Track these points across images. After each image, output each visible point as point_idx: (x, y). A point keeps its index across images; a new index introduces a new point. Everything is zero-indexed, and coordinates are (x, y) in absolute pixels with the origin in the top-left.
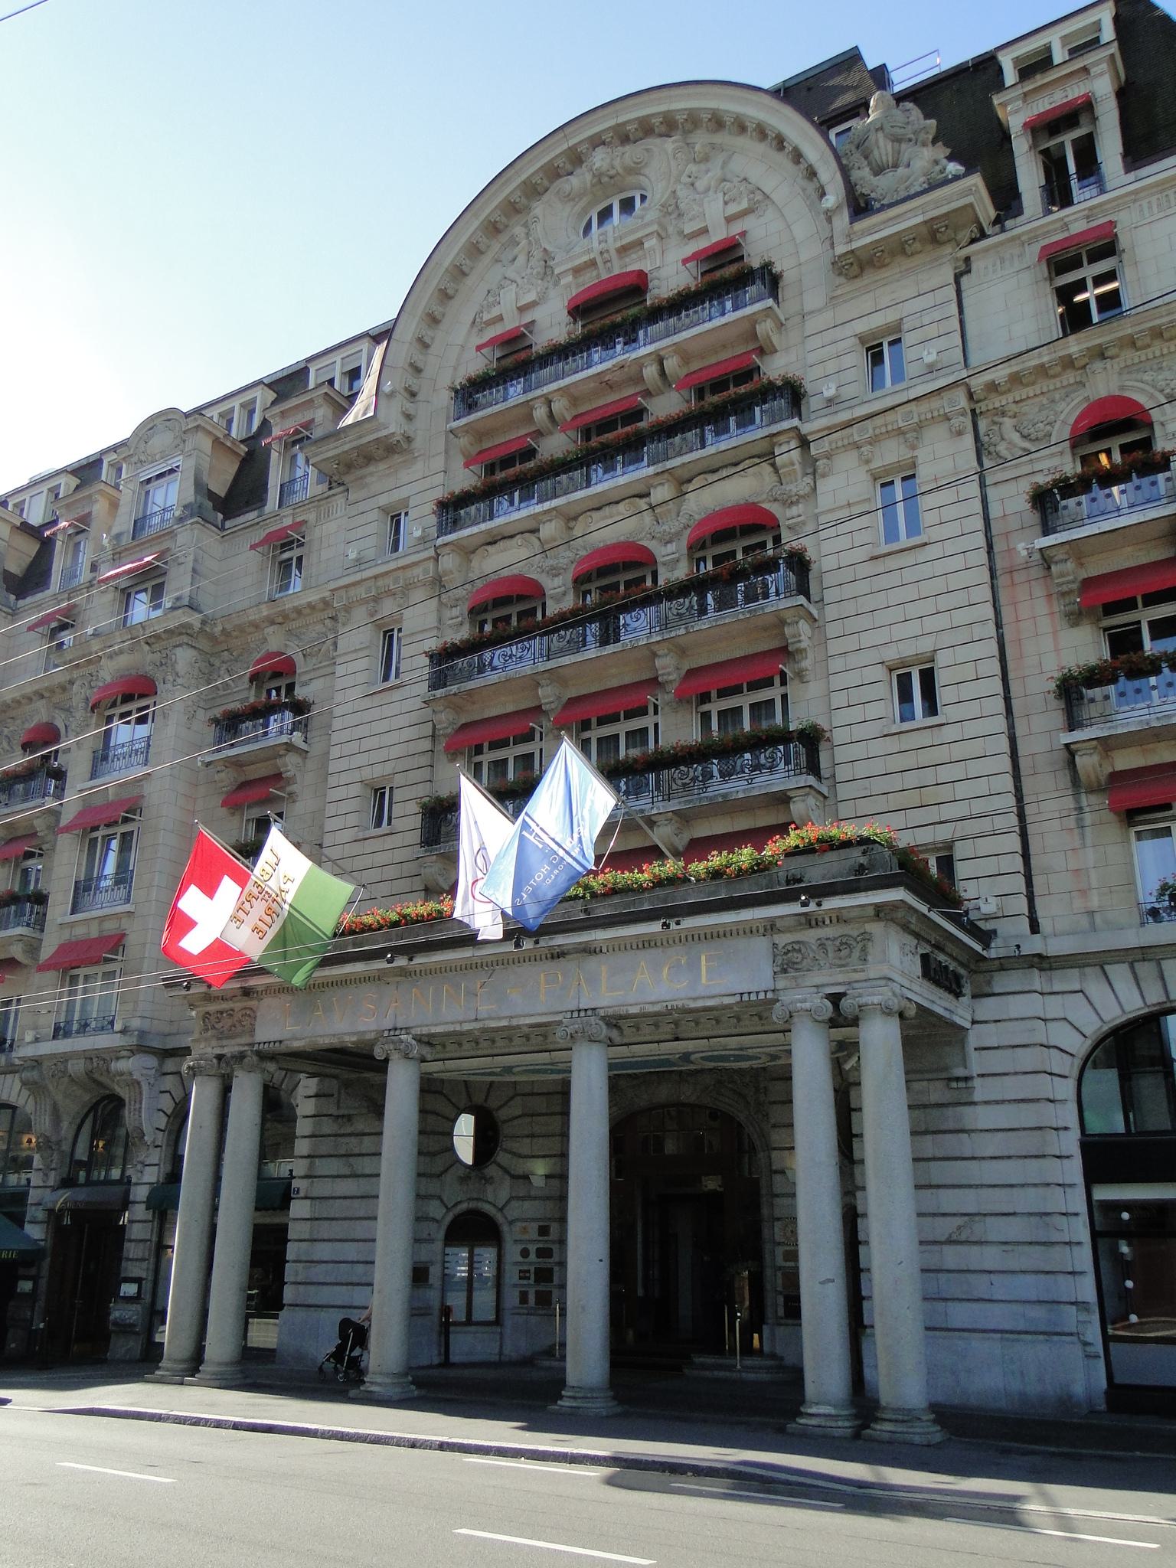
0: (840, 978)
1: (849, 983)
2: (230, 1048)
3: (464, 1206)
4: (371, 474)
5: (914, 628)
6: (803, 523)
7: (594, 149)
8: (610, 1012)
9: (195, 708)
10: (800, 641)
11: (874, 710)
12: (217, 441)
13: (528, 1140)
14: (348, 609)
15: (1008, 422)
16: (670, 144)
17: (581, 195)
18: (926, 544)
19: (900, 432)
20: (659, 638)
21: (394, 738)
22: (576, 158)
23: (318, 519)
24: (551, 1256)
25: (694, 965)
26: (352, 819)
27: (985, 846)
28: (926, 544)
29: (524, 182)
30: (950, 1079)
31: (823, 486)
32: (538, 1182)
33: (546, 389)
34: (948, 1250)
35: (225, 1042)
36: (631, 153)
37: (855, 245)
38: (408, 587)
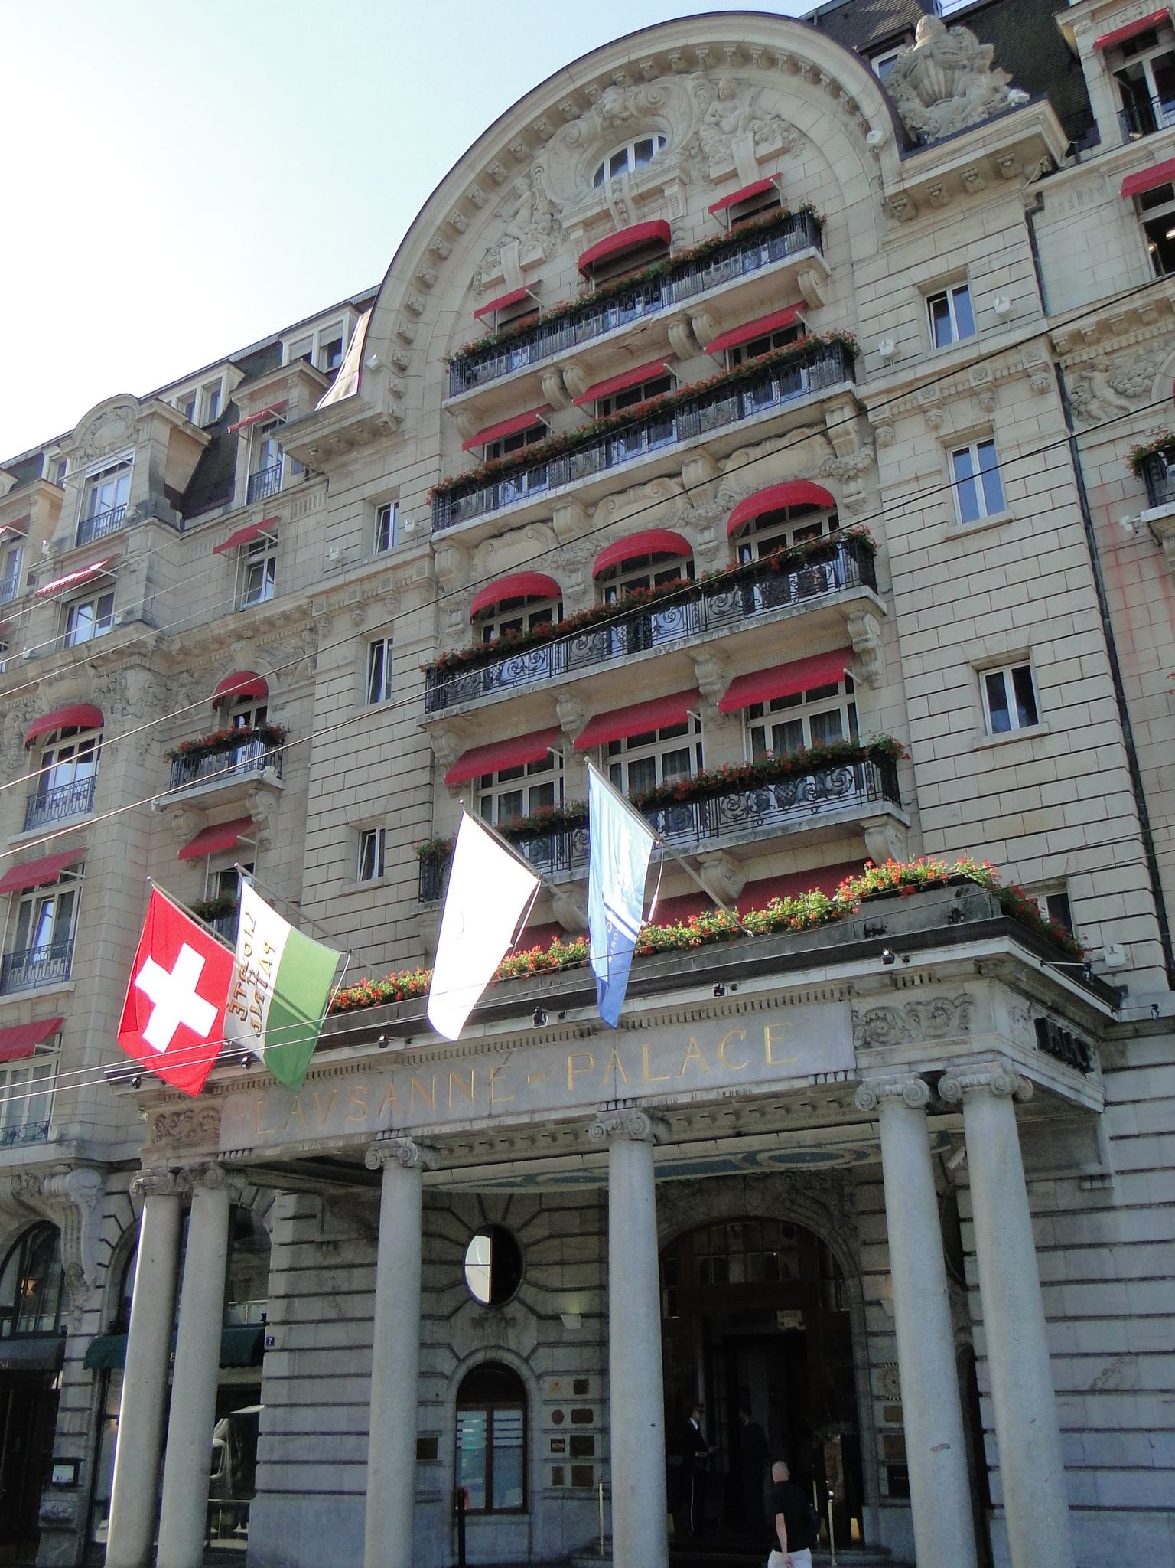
0: (937, 1052)
1: (948, 1059)
2: (188, 1160)
3: (479, 1357)
4: (355, 461)
5: (1001, 620)
6: (864, 501)
7: (604, 90)
8: (655, 1102)
9: (149, 741)
10: (867, 640)
11: (959, 720)
12: (175, 430)
13: (558, 1269)
14: (329, 618)
15: (1099, 377)
16: (690, 82)
17: (590, 141)
18: (1011, 521)
19: (973, 393)
20: (698, 642)
21: (385, 769)
22: (584, 101)
23: (293, 515)
24: (590, 1420)
25: (756, 1042)
26: (336, 870)
27: (1106, 882)
28: (1011, 521)
29: (525, 129)
30: (1082, 1178)
31: (885, 457)
32: (571, 1323)
33: (556, 358)
34: (1094, 1402)
35: (182, 1152)
36: (644, 94)
37: (907, 184)
38: (398, 592)
